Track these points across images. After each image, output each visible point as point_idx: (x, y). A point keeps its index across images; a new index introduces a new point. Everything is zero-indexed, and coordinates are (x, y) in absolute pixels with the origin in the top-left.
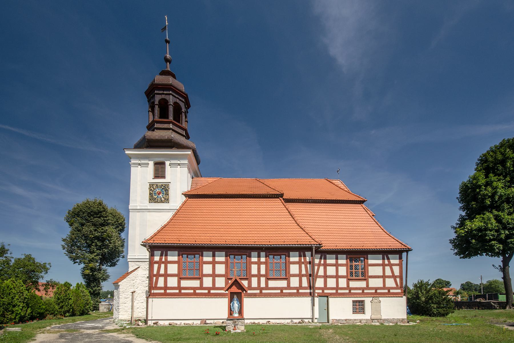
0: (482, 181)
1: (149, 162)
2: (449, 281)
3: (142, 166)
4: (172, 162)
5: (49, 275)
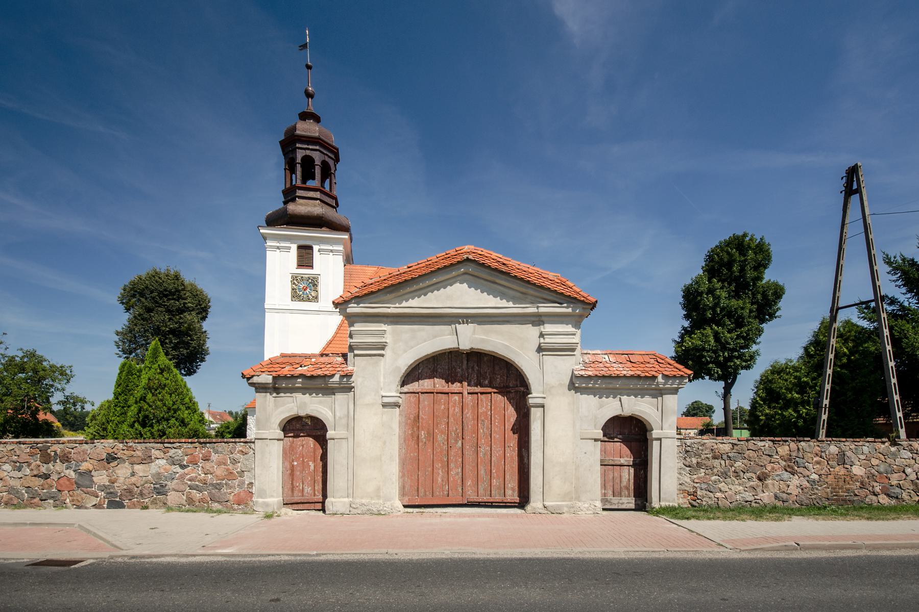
0: (704, 288)
1: (291, 245)
2: (711, 406)
3: (281, 250)
5: (72, 386)
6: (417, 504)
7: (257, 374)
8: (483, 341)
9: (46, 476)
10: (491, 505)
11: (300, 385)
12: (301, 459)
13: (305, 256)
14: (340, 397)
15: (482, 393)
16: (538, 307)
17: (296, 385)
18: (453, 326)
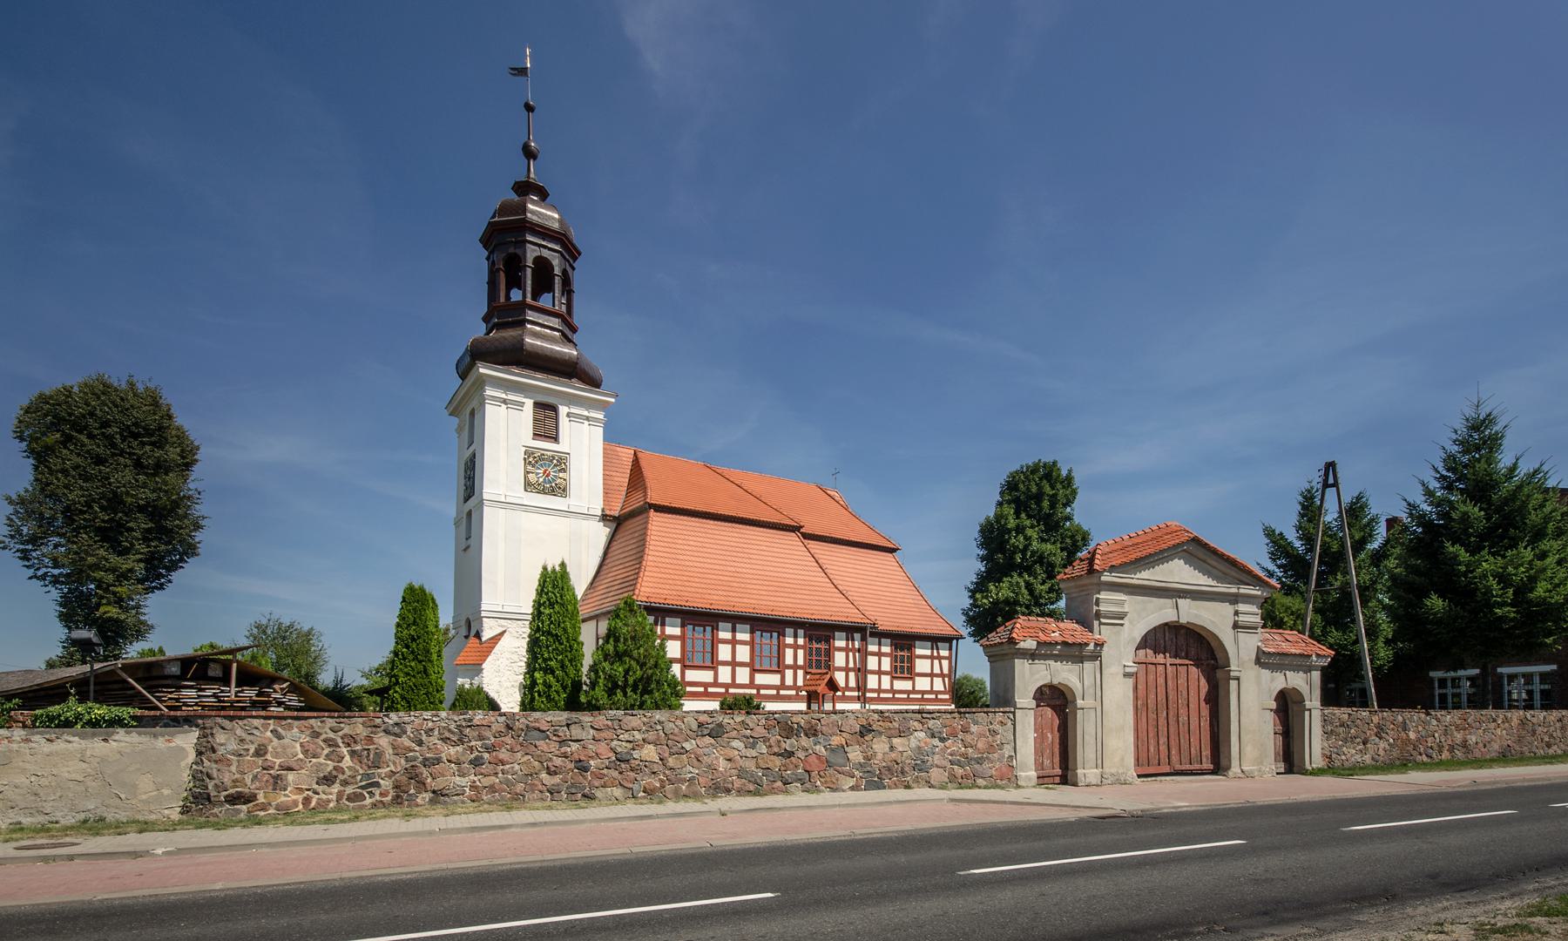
1: (524, 400)
4: (573, 410)
8: (1196, 615)
9: (790, 754)
10: (1192, 773)
13: (546, 425)
14: (1088, 665)
16: (1238, 588)
18: (1174, 600)
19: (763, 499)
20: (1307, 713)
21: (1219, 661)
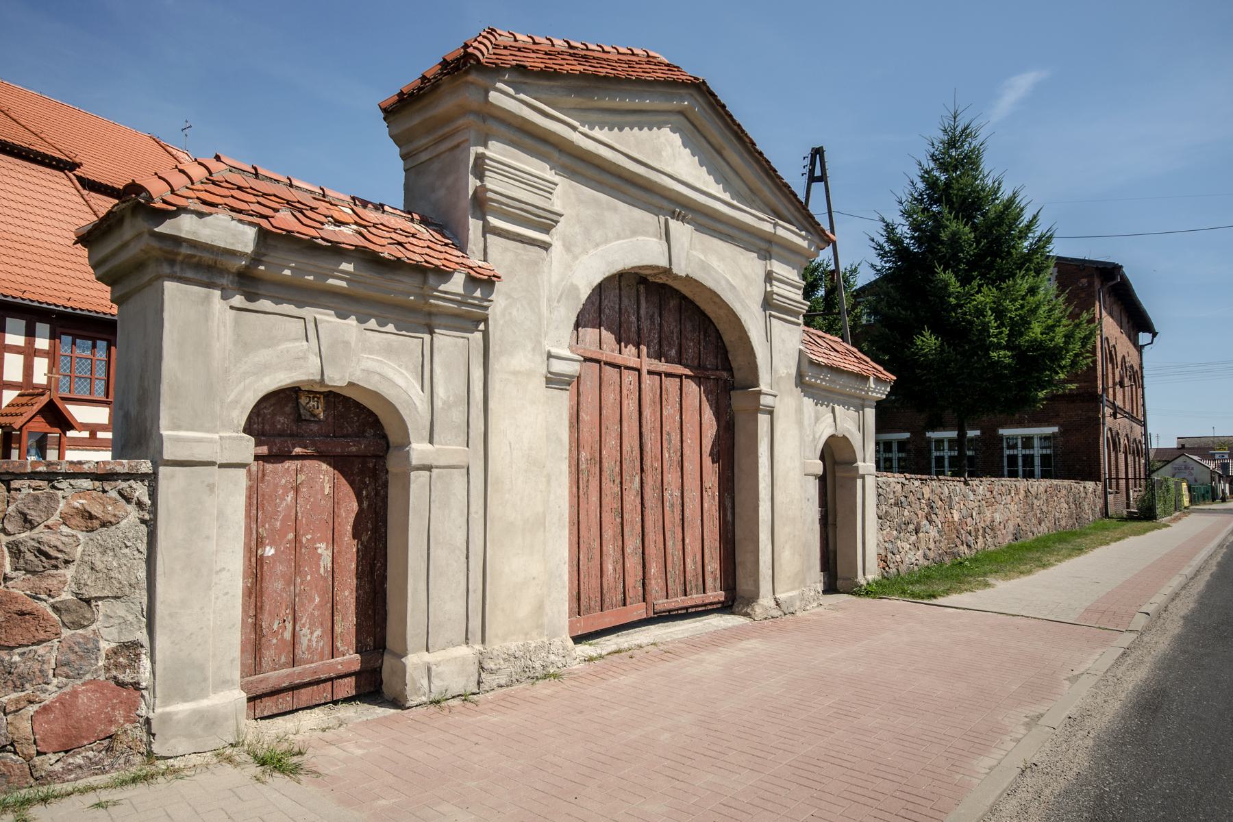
6: (579, 633)
7: (194, 205)
11: (344, 284)
12: (291, 536)
14: (447, 342)
15: (668, 375)
17: (331, 281)
19: (12, 115)
20: (859, 482)
21: (735, 372)
